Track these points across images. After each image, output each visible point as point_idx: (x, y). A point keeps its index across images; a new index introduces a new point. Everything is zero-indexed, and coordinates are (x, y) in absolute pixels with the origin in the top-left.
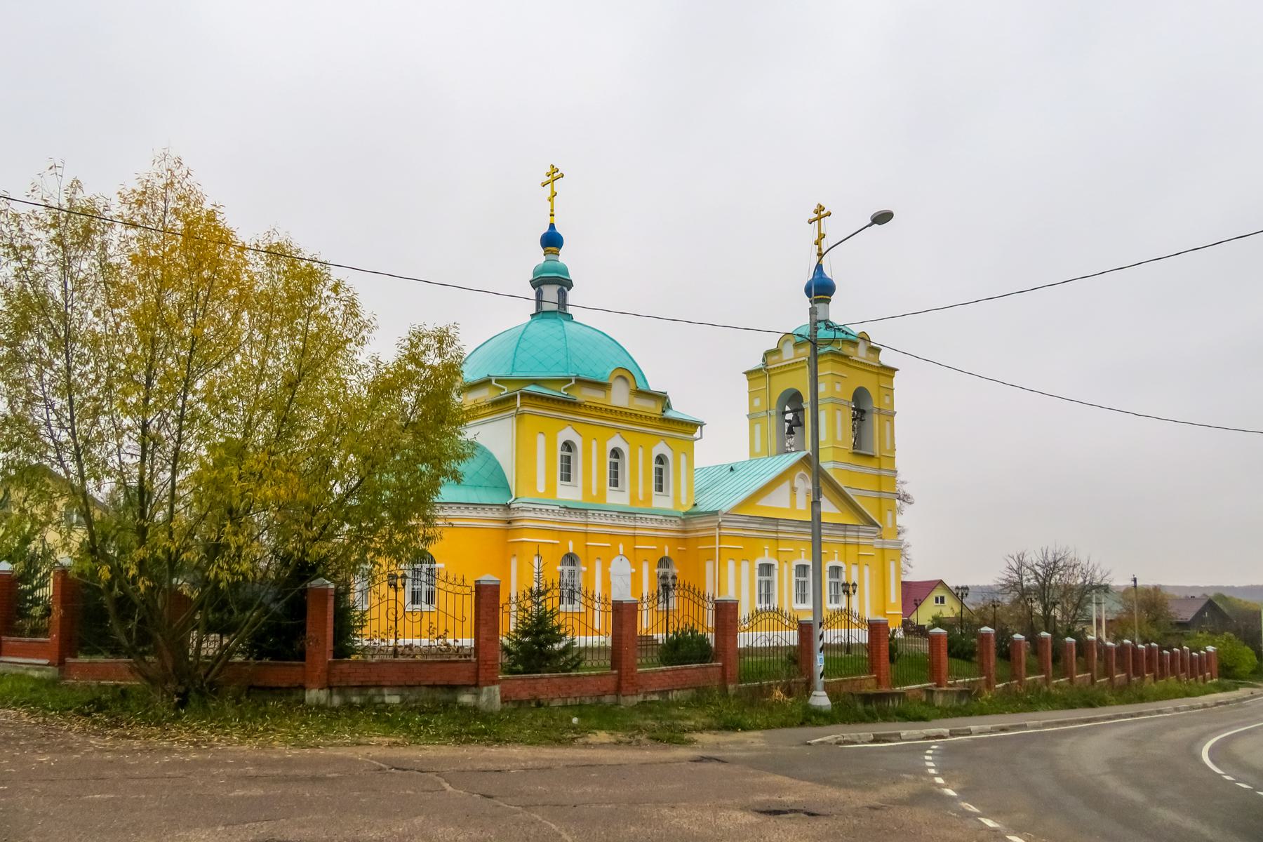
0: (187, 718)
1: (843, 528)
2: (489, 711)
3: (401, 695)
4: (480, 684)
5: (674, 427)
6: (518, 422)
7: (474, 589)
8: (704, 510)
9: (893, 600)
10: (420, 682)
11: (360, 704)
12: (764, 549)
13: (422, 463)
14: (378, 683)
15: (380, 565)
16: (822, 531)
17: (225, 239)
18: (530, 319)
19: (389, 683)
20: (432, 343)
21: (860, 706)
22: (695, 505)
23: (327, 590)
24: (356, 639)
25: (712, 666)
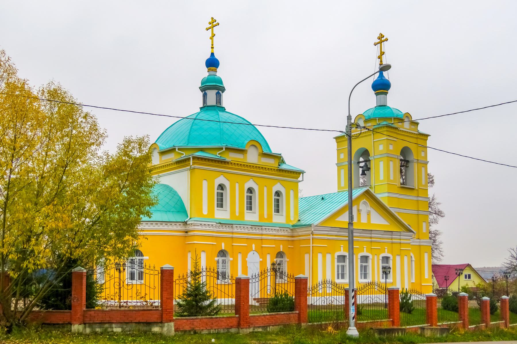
0: (13, 338)
1: (390, 233)
2: (168, 336)
3: (122, 328)
4: (163, 321)
5: (342, 140)
6: (191, 173)
7: (160, 272)
8: (304, 224)
9: (426, 276)
10: (131, 321)
11: (100, 332)
12: (385, 248)
13: (131, 208)
14: (110, 322)
15: (110, 260)
16: (354, 234)
17: (29, 95)
18: (199, 110)
19: (115, 321)
20: (136, 145)
21: (377, 335)
22: (299, 220)
23: (82, 273)
24: (98, 299)
25: (293, 313)
